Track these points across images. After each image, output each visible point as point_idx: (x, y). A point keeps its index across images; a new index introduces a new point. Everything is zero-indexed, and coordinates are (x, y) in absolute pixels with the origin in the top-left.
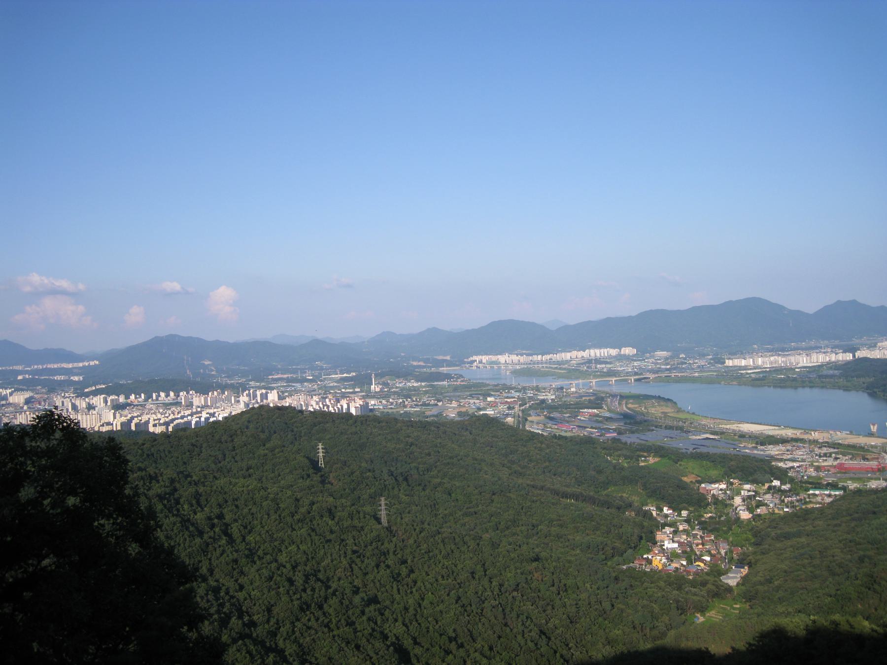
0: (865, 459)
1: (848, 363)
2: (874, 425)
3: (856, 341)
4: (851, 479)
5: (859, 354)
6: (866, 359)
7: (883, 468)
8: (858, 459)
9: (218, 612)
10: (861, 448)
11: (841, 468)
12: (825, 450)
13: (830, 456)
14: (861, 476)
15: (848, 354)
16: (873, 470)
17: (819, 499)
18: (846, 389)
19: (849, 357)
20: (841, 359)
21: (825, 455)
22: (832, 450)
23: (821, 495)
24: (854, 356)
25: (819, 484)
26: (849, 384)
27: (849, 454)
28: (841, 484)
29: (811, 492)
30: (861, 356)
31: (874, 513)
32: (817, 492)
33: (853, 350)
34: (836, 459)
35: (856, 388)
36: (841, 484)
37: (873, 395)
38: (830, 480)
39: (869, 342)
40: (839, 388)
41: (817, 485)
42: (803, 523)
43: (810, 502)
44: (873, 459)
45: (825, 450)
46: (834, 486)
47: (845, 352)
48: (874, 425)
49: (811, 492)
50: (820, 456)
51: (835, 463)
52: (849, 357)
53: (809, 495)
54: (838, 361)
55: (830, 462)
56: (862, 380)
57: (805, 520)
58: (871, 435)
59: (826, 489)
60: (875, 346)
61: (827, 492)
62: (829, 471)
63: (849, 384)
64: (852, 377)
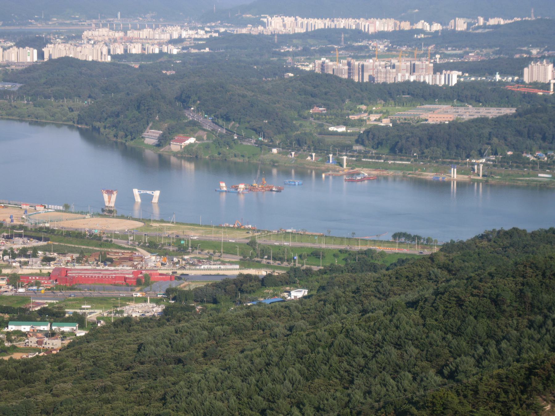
0: (106, 260)
1: (32, 68)
2: (110, 192)
3: (36, 26)
4: (89, 300)
5: (56, 50)
6: (67, 61)
7: (147, 277)
8: (91, 260)
9: (465, 266)
10: (95, 239)
11: (63, 281)
12: (18, 244)
13: (35, 255)
14: (106, 294)
15: (28, 50)
16: (126, 283)
17: (32, 342)
18: (37, 122)
19: (30, 56)
20: (13, 59)
21: (23, 253)
22: (35, 243)
23: (34, 333)
24: (41, 55)
25: (24, 310)
26: (40, 111)
27: (72, 251)
28: (69, 312)
29: (12, 328)
30: (55, 56)
31: (179, 361)
32: (25, 328)
33: (38, 43)
34: (47, 260)
35: (57, 121)
36: (69, 312)
37: (91, 135)
38: (46, 303)
39: (64, 29)
40: (21, 119)
41: (24, 315)
42: (26, 390)
43: (14, 349)
44: (122, 260)
45: (18, 244)
46: (53, 315)
47: (21, 44)
48: (110, 192)
49: (12, 328)
50: (14, 256)
51: (49, 269)
52: (30, 56)
53: (8, 333)
54: (9, 64)
55: (34, 267)
56: (66, 103)
57: (28, 382)
58: (108, 213)
59: (43, 320)
60: (79, 37)
61: (46, 328)
62: (38, 284)
63: (40, 111)
64: (47, 97)
